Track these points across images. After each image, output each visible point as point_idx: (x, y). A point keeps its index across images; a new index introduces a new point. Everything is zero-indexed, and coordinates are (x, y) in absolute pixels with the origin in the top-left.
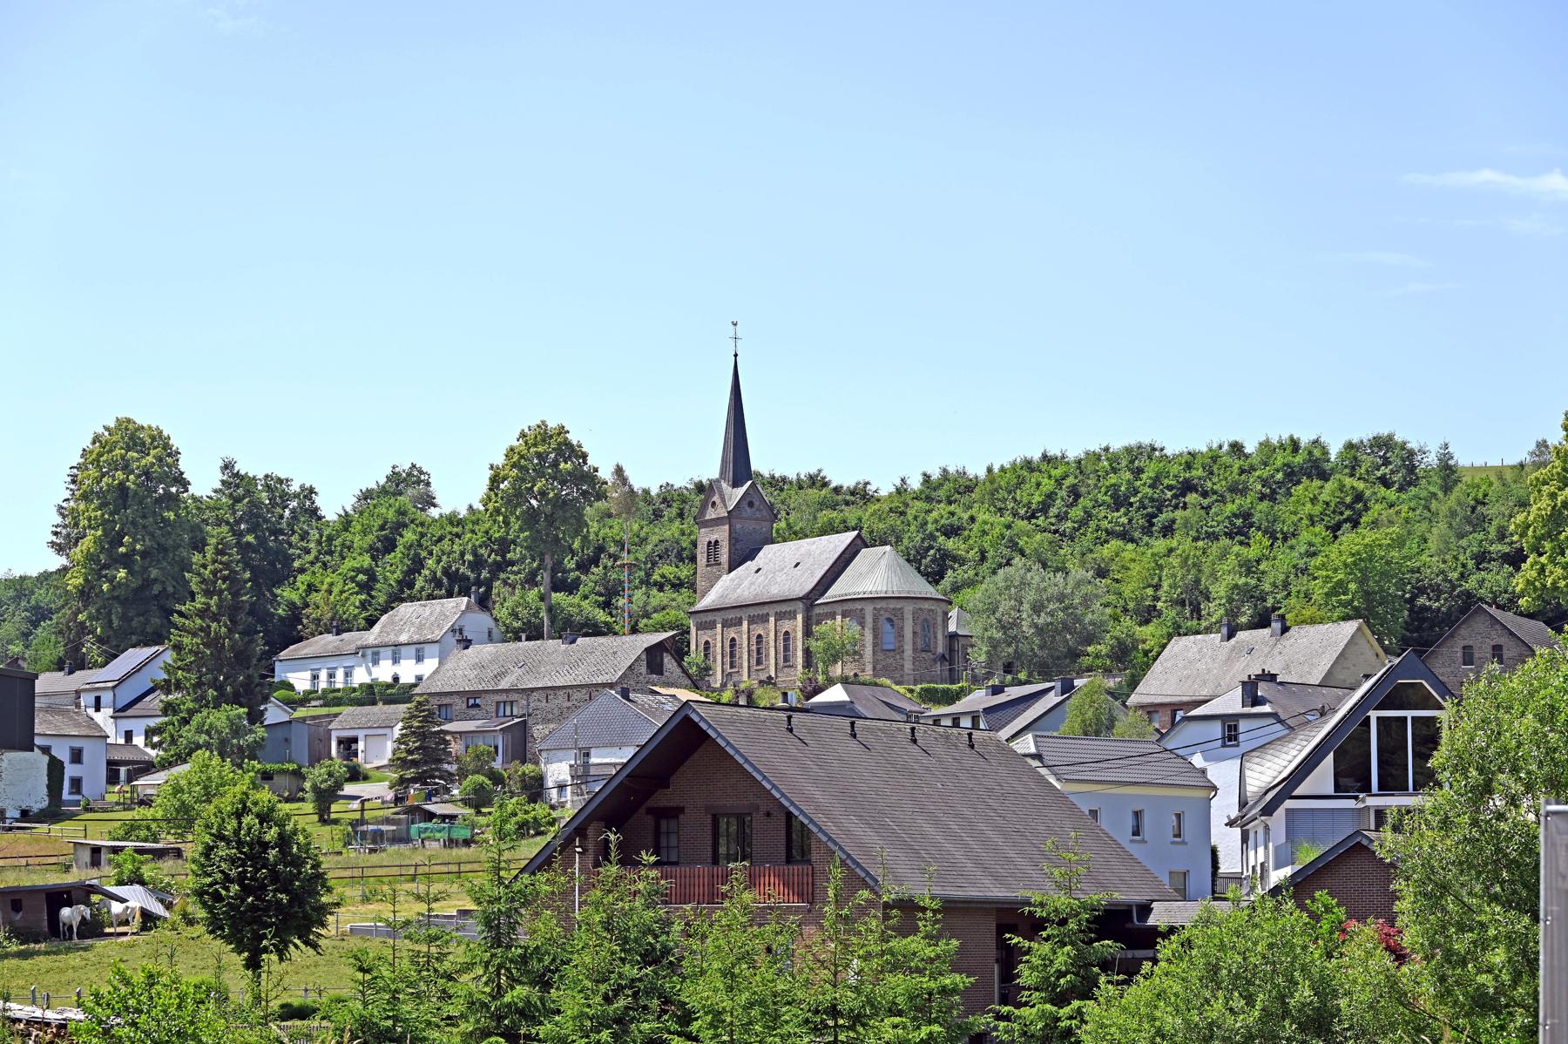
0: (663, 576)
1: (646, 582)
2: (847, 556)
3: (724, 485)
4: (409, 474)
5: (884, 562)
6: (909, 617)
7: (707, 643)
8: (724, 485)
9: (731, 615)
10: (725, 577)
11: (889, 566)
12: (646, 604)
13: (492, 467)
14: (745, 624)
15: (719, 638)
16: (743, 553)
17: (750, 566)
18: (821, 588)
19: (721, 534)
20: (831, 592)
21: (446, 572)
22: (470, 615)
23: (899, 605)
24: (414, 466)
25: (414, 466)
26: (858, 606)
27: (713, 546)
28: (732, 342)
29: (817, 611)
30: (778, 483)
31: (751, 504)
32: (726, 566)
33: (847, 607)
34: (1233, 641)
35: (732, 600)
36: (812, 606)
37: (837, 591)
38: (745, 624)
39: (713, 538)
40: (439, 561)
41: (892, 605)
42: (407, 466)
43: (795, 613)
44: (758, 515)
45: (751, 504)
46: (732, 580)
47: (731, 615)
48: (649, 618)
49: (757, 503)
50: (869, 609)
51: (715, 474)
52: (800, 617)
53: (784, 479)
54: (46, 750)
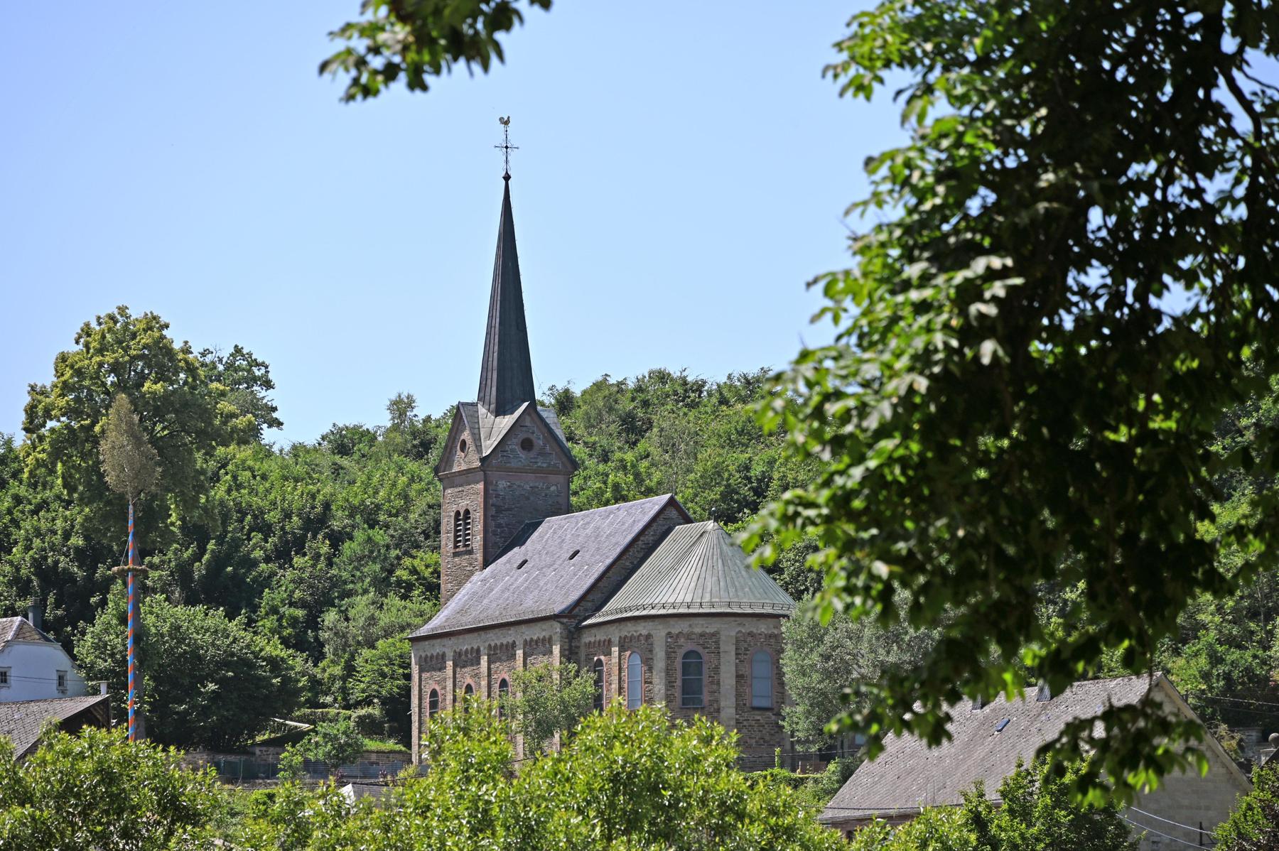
0: (414, 571)
1: (383, 584)
2: (649, 538)
3: (482, 410)
4: (230, 366)
5: (699, 550)
6: (728, 649)
7: (434, 693)
8: (482, 410)
9: (465, 644)
10: (477, 577)
11: (704, 559)
12: (372, 620)
13: (33, 388)
14: (484, 661)
15: (449, 684)
16: (508, 531)
17: (516, 554)
18: (597, 596)
19: (472, 498)
20: (613, 604)
21: (38, 564)
22: (20, 648)
23: (711, 627)
24: (238, 350)
25: (238, 350)
26: (643, 629)
27: (463, 518)
28: (500, 154)
29: (587, 638)
30: (565, 403)
31: (527, 445)
32: (479, 556)
33: (630, 629)
34: (987, 709)
35: (468, 622)
36: (579, 629)
37: (618, 604)
38: (484, 661)
39: (463, 504)
40: (28, 548)
41: (699, 627)
42: (225, 354)
43: (549, 641)
44: (541, 463)
45: (527, 445)
46: (484, 580)
47: (465, 644)
48: (373, 647)
49: (539, 442)
50: (659, 633)
51: (472, 396)
52: (556, 650)
53: (699, 387)
54: (1190, 729)
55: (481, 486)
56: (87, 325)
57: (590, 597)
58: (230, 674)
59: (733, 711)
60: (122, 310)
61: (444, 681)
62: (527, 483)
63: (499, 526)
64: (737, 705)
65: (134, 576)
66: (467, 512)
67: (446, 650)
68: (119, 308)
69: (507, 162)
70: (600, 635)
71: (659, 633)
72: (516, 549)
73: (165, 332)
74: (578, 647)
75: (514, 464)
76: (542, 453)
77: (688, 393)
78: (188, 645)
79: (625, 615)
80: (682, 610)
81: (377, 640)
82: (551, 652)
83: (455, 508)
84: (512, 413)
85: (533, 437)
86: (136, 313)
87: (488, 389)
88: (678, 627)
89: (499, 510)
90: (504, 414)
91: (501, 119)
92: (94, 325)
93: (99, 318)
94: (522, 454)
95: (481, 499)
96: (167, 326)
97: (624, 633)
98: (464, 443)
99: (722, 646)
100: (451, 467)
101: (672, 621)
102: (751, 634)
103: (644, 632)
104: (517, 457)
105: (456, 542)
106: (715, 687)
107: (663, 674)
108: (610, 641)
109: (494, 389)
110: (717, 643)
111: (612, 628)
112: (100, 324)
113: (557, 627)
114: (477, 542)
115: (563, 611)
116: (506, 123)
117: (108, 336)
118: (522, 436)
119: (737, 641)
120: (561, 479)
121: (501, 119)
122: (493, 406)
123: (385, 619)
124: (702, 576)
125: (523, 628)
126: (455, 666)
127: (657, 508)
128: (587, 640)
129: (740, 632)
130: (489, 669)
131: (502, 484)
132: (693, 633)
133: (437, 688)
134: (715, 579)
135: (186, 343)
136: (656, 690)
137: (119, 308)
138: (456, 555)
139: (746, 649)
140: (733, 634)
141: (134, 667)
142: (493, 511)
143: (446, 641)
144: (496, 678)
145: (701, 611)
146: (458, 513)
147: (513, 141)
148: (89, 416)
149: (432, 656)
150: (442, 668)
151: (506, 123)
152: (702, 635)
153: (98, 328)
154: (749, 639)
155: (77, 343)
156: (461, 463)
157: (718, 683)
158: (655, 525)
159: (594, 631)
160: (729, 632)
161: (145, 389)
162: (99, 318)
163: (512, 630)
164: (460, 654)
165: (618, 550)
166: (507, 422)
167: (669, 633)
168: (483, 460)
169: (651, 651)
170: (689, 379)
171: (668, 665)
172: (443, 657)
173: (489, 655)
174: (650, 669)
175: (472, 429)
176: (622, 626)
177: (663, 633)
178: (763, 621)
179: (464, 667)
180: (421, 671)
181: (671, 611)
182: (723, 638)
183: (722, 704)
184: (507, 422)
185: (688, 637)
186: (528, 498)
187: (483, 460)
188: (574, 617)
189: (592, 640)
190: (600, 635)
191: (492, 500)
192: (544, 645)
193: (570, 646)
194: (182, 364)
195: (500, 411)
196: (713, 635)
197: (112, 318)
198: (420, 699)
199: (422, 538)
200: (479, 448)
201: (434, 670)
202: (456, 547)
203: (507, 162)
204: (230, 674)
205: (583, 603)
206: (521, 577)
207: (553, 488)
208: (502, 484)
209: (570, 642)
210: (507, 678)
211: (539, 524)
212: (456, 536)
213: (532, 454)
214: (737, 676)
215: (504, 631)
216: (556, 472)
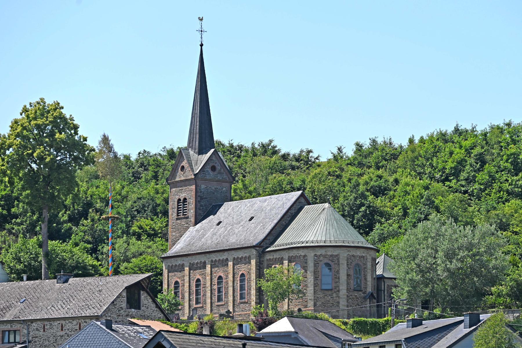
0: (140, 227)
1: (126, 232)
2: (293, 211)
3: (191, 152)
6: (343, 263)
7: (177, 283)
8: (191, 152)
9: (196, 260)
10: (191, 229)
12: (127, 250)
14: (208, 267)
16: (207, 208)
18: (271, 238)
19: (189, 193)
23: (336, 252)
26: (302, 253)
28: (198, 34)
29: (268, 257)
31: (213, 168)
32: (193, 220)
35: (194, 249)
36: (264, 252)
37: (283, 241)
39: (182, 196)
41: (330, 252)
43: (249, 258)
44: (219, 177)
45: (213, 168)
48: (129, 262)
49: (218, 168)
52: (253, 262)
53: (241, 148)
55: (193, 187)
56: (25, 106)
57: (268, 238)
58: (80, 272)
59: (346, 291)
60: (42, 100)
61: (185, 278)
62: (214, 186)
63: (201, 206)
64: (347, 288)
65: (112, 220)
66: (185, 199)
67: (184, 263)
68: (41, 99)
69: (201, 38)
70: (276, 256)
71: (311, 255)
72: (212, 217)
73: (62, 110)
74: (263, 261)
75: (208, 177)
76: (220, 173)
77: (443, 137)
78: (60, 258)
79: (292, 246)
80: (321, 244)
81: (131, 259)
82: (250, 263)
83: (177, 197)
84: (206, 153)
85: (216, 165)
86: (49, 101)
87: (194, 143)
88: (319, 252)
89: (202, 198)
90: (202, 154)
91: (199, 18)
92: (28, 106)
93: (30, 103)
94: (211, 173)
95: (193, 193)
96: (62, 108)
97: (291, 255)
98: (183, 167)
99: (340, 261)
100: (175, 178)
101: (317, 249)
102: (353, 256)
103: (303, 254)
104: (209, 174)
105: (178, 213)
106: (337, 280)
107: (313, 274)
108: (282, 258)
109: (197, 142)
110: (338, 259)
111: (285, 252)
112: (31, 106)
113: (254, 252)
114: (191, 213)
115: (257, 244)
116: (201, 19)
117: (38, 111)
118: (211, 164)
119: (348, 259)
120: (227, 185)
121: (199, 18)
122: (197, 150)
123: (133, 249)
124: (328, 228)
125: (233, 252)
126: (190, 270)
127: (294, 200)
128: (268, 258)
129: (349, 254)
130: (211, 271)
131: (203, 186)
132: (327, 255)
133: (179, 280)
134: (334, 230)
135: (71, 116)
136: (309, 281)
137: (41, 99)
138: (177, 219)
139: (351, 263)
140: (346, 255)
141: (45, 268)
142: (199, 199)
143: (184, 258)
144: (216, 276)
145: (331, 244)
146: (179, 200)
147: (204, 28)
148: (30, 149)
149: (176, 265)
150: (205, 267)
151: (201, 19)
152: (331, 256)
153: (30, 108)
154: (353, 258)
155: (21, 115)
156: (180, 177)
157: (339, 278)
158: (295, 205)
159: (272, 254)
160: (344, 254)
161: (56, 137)
162: (30, 103)
163: (226, 253)
164: (193, 264)
165: (280, 216)
166: (206, 157)
167: (316, 255)
168: (195, 175)
169: (306, 263)
170: (235, 145)
171: (315, 269)
172: (205, 263)
173: (211, 265)
174: (306, 271)
175: (188, 161)
176: (290, 251)
177: (313, 255)
178: (358, 249)
179: (195, 270)
180: (169, 272)
181: (316, 244)
182: (341, 257)
183: (341, 288)
184: (206, 157)
185: (325, 256)
186: (214, 193)
187: (195, 175)
188: (262, 247)
189: (272, 257)
190: (276, 256)
191: (199, 194)
192: (245, 260)
193: (260, 260)
194: (72, 125)
195: (201, 152)
196: (337, 256)
197: (38, 103)
198: (168, 285)
199: (136, 213)
200: (192, 169)
201: (176, 271)
202: (178, 216)
203: (201, 38)
204: (80, 272)
205: (265, 241)
206: (221, 229)
207: (224, 189)
208: (203, 186)
209: (260, 259)
210: (222, 275)
211: (221, 205)
212: (178, 211)
213: (216, 173)
214: (347, 275)
215: (221, 253)
216: (226, 182)
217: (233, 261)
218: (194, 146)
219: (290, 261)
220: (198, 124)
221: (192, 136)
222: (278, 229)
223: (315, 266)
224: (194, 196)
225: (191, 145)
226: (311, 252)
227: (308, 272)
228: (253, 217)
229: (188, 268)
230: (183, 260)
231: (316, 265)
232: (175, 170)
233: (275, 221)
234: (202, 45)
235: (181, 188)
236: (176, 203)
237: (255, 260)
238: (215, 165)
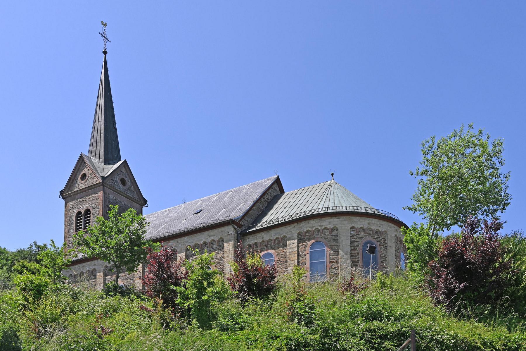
2: (269, 196)
26: (328, 223)
29: (251, 240)
39: (83, 209)
55: (101, 194)
66: (88, 211)
83: (76, 211)
95: (100, 201)
116: (105, 25)
122: (101, 160)
132: (370, 229)
169: (336, 240)
189: (259, 241)
190: (272, 235)
217: (186, 252)
218: (97, 155)
219: (301, 240)
220: (103, 131)
221: (94, 144)
222: (262, 205)
223: (352, 245)
224: (101, 204)
225: (93, 154)
226: (346, 222)
227: (341, 252)
228: (201, 210)
229: (102, 274)
230: (95, 265)
231: (353, 244)
232: (73, 181)
233: (251, 203)
234: (105, 53)
235: (81, 200)
236: (74, 218)
237: (232, 243)
238: (125, 178)
